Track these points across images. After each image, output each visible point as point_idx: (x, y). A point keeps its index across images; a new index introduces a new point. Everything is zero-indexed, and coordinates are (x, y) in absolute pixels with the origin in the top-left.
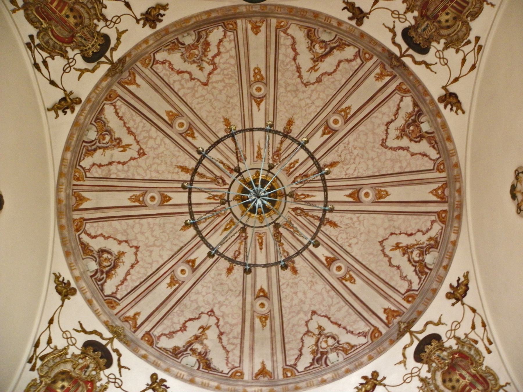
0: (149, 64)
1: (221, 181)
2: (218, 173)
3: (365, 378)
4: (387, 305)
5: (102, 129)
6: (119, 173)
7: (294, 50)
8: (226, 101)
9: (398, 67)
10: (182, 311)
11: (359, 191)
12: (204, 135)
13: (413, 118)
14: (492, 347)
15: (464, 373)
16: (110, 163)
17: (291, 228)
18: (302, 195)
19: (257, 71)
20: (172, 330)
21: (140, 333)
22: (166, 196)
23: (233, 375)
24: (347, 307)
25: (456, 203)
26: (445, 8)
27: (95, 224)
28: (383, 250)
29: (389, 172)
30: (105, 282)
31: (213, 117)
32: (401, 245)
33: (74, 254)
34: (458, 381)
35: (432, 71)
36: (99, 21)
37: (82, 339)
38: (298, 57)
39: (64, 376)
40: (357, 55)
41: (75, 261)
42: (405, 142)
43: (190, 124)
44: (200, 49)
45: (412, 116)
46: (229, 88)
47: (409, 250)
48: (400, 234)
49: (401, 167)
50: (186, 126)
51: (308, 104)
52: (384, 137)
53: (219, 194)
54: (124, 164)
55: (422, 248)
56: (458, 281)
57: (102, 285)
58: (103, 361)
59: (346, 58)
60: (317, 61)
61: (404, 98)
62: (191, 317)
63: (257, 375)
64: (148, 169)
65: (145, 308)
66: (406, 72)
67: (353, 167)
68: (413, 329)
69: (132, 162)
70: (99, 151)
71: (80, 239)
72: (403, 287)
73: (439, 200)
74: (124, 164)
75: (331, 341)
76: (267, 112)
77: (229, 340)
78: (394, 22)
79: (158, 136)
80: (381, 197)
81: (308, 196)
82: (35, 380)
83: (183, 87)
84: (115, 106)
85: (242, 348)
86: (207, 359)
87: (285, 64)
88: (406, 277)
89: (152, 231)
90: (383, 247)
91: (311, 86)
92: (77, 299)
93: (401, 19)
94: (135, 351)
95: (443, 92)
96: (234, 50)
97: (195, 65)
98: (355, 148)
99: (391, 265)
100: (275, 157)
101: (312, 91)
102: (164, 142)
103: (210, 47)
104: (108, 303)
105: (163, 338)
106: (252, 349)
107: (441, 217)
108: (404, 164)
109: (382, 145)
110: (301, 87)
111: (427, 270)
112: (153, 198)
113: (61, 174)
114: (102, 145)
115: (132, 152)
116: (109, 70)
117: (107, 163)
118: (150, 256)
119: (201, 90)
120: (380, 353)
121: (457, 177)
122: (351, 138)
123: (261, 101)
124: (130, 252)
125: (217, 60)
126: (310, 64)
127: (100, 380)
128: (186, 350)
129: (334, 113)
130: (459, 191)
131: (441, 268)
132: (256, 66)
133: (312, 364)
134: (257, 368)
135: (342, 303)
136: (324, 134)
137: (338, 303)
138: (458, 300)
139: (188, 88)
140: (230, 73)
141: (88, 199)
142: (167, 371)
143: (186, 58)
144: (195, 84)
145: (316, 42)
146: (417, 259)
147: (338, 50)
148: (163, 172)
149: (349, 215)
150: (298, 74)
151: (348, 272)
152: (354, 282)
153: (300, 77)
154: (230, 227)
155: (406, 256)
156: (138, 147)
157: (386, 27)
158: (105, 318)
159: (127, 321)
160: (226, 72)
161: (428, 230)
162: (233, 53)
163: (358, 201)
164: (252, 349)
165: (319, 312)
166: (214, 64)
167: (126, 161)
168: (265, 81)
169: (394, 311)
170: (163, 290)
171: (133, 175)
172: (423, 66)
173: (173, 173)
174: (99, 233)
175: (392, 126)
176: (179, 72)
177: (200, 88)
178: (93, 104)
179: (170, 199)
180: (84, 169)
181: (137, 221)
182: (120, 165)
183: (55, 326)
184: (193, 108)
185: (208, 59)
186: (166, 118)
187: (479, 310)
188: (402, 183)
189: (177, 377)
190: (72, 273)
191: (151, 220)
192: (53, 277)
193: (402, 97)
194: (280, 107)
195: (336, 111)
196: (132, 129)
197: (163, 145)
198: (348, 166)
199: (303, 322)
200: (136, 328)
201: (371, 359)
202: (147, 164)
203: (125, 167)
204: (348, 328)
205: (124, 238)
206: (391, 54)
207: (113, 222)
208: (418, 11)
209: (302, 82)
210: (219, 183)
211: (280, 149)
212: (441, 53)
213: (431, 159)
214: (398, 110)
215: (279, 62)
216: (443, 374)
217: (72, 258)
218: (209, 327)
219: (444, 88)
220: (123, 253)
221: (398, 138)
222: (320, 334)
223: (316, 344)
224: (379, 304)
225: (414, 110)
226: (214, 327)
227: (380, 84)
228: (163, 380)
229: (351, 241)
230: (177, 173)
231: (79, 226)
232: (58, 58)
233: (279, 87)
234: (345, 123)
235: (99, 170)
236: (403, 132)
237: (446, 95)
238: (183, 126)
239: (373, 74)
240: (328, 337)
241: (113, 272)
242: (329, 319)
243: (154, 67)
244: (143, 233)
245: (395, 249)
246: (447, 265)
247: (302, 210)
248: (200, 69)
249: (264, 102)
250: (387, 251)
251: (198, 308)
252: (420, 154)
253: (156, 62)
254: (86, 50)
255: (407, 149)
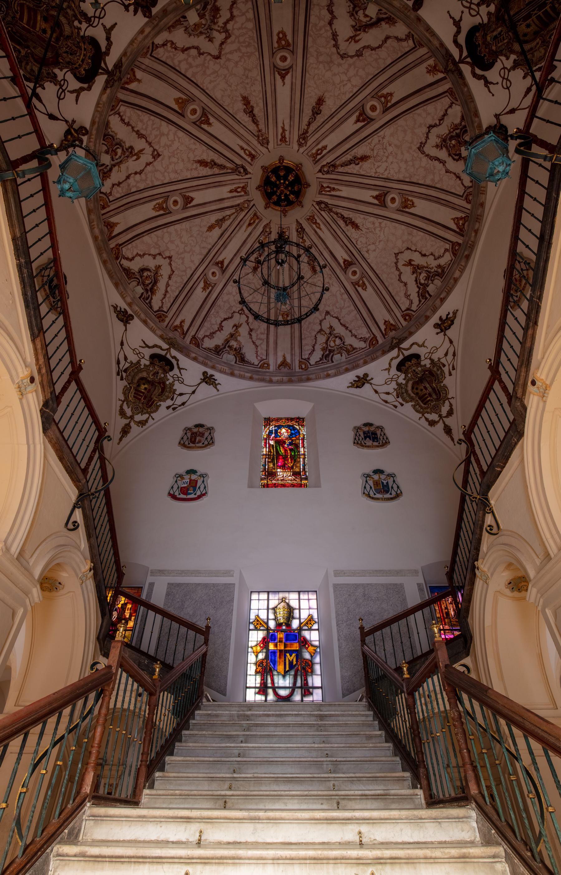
0: (148, 51)
1: (242, 171)
2: (238, 161)
3: (357, 377)
4: (388, 317)
5: (112, 144)
6: (138, 185)
7: (331, 12)
8: (244, 75)
9: (453, 72)
10: (218, 312)
11: (385, 195)
12: (221, 120)
13: (458, 131)
14: (453, 372)
15: (428, 386)
16: (128, 177)
17: (314, 223)
18: (328, 187)
19: (282, 35)
20: (212, 331)
21: (188, 339)
22: (188, 197)
23: (262, 367)
24: (355, 312)
25: (470, 242)
26: (529, 16)
27: (130, 246)
28: (396, 263)
29: (420, 182)
30: (152, 299)
31: (229, 96)
32: (413, 263)
33: (122, 284)
34: (422, 390)
35: (490, 91)
36: (80, 23)
37: (147, 353)
38: (335, 21)
39: (144, 381)
40: (409, 36)
41: (125, 289)
42: (443, 154)
43: (204, 109)
44: (207, 17)
45: (457, 129)
46: (246, 58)
47: (418, 271)
48: (415, 251)
49: (433, 180)
50: (199, 112)
51: (343, 81)
52: (424, 141)
53: (241, 185)
54: (140, 173)
55: (430, 272)
56: (447, 315)
57: (150, 302)
58: (167, 368)
59: (396, 35)
60: (360, 30)
61: (454, 105)
62: (226, 317)
63: (280, 366)
64: (165, 171)
65: (187, 314)
66: (460, 81)
67: (384, 165)
68: (401, 346)
69: (149, 168)
70: (115, 169)
71: (121, 266)
72: (404, 304)
73: (458, 230)
74: (140, 173)
75: (338, 341)
76: (294, 87)
77: (257, 335)
78: (462, 12)
79: (169, 131)
80: (406, 207)
81: (334, 189)
82: (126, 386)
83: (191, 66)
84: (119, 114)
85: (268, 342)
86: (242, 354)
87: (318, 28)
88: (409, 295)
89: (181, 238)
90: (397, 259)
91: (349, 58)
92: (136, 323)
93: (471, 11)
94: (187, 356)
95: (494, 121)
96: (251, 11)
97: (202, 37)
98: (390, 145)
99: (400, 280)
100: (301, 140)
101: (350, 65)
102: (178, 137)
103: (220, 12)
104: (158, 318)
105: (206, 339)
106: (276, 343)
107: (455, 249)
108: (437, 179)
109: (419, 148)
110: (336, 58)
111: (427, 296)
112: (176, 202)
113: (89, 211)
114: (116, 161)
115: (146, 157)
116: (107, 82)
117: (124, 178)
118: (183, 263)
119: (213, 65)
120: (373, 360)
121: (479, 217)
122: (387, 131)
123: (287, 74)
124: (164, 263)
125: (229, 26)
126: (350, 33)
127: (168, 380)
128: (225, 348)
129: (373, 97)
130: (476, 232)
131: (438, 300)
132: (281, 30)
133: (321, 359)
134: (280, 360)
135: (352, 308)
136: (358, 121)
137: (348, 307)
138: (442, 331)
139: (197, 66)
140: (247, 40)
141: (118, 223)
142: (213, 367)
143: (191, 32)
144: (205, 60)
145: (360, 7)
146: (422, 281)
147: (387, 23)
148: (181, 171)
149: (372, 219)
150: (334, 42)
151: (362, 278)
152: (365, 289)
153: (336, 46)
154: (254, 222)
155: (415, 275)
156: (152, 149)
157: (451, 17)
158: (159, 332)
159: (176, 330)
160: (242, 39)
161: (440, 257)
162: (250, 15)
163: (383, 204)
164: (276, 343)
165: (332, 313)
166: (227, 31)
167: (142, 169)
168: (291, 48)
169: (392, 324)
170: (199, 294)
171: (152, 181)
172: (482, 81)
173: (191, 170)
174: (135, 253)
175: (434, 131)
176: (184, 50)
177: (211, 63)
178: (98, 126)
179: (192, 199)
180: (105, 194)
181: (165, 230)
182: (138, 175)
183: (125, 347)
184: (205, 88)
185: (218, 26)
186: (176, 107)
187: (455, 343)
188: (430, 198)
189: (221, 371)
190: (125, 301)
191: (178, 227)
192: (112, 308)
193: (452, 103)
194: (309, 82)
195: (375, 95)
196: (143, 132)
197: (177, 139)
198: (379, 164)
199: (318, 321)
200: (184, 334)
201: (366, 363)
202: (164, 166)
203: (143, 175)
204: (353, 332)
205: (157, 251)
206: (448, 55)
207: (144, 238)
208: (496, 6)
209: (338, 53)
210: (240, 172)
211: (307, 132)
212: (506, 71)
213: (463, 185)
214: (444, 115)
215: (311, 25)
216: (413, 384)
217: (121, 287)
218: (241, 325)
219: (497, 116)
220: (160, 266)
221: (437, 146)
222: (330, 333)
223: (326, 343)
224: (382, 315)
225: (461, 123)
226: (245, 325)
227: (431, 79)
228: (212, 375)
229: (369, 247)
230: (196, 169)
231: (117, 253)
232: (47, 85)
233: (308, 55)
234: (384, 112)
235: (119, 189)
236: (443, 143)
237: (496, 125)
238: (196, 113)
239: (425, 65)
240: (336, 337)
241: (155, 288)
242: (339, 320)
243: (154, 54)
244: (172, 242)
245: (407, 266)
246: (444, 298)
247: (326, 204)
248: (209, 40)
249: (289, 75)
250: (400, 265)
251: (231, 307)
252: (455, 174)
253: (155, 47)
254: (76, 68)
255: (443, 162)
